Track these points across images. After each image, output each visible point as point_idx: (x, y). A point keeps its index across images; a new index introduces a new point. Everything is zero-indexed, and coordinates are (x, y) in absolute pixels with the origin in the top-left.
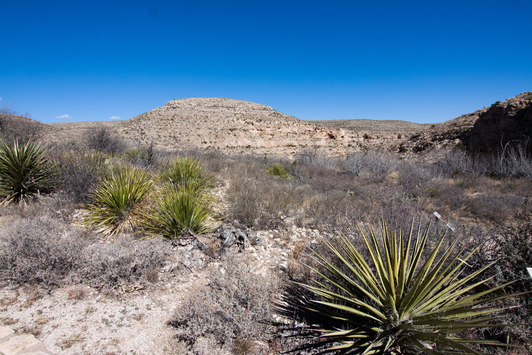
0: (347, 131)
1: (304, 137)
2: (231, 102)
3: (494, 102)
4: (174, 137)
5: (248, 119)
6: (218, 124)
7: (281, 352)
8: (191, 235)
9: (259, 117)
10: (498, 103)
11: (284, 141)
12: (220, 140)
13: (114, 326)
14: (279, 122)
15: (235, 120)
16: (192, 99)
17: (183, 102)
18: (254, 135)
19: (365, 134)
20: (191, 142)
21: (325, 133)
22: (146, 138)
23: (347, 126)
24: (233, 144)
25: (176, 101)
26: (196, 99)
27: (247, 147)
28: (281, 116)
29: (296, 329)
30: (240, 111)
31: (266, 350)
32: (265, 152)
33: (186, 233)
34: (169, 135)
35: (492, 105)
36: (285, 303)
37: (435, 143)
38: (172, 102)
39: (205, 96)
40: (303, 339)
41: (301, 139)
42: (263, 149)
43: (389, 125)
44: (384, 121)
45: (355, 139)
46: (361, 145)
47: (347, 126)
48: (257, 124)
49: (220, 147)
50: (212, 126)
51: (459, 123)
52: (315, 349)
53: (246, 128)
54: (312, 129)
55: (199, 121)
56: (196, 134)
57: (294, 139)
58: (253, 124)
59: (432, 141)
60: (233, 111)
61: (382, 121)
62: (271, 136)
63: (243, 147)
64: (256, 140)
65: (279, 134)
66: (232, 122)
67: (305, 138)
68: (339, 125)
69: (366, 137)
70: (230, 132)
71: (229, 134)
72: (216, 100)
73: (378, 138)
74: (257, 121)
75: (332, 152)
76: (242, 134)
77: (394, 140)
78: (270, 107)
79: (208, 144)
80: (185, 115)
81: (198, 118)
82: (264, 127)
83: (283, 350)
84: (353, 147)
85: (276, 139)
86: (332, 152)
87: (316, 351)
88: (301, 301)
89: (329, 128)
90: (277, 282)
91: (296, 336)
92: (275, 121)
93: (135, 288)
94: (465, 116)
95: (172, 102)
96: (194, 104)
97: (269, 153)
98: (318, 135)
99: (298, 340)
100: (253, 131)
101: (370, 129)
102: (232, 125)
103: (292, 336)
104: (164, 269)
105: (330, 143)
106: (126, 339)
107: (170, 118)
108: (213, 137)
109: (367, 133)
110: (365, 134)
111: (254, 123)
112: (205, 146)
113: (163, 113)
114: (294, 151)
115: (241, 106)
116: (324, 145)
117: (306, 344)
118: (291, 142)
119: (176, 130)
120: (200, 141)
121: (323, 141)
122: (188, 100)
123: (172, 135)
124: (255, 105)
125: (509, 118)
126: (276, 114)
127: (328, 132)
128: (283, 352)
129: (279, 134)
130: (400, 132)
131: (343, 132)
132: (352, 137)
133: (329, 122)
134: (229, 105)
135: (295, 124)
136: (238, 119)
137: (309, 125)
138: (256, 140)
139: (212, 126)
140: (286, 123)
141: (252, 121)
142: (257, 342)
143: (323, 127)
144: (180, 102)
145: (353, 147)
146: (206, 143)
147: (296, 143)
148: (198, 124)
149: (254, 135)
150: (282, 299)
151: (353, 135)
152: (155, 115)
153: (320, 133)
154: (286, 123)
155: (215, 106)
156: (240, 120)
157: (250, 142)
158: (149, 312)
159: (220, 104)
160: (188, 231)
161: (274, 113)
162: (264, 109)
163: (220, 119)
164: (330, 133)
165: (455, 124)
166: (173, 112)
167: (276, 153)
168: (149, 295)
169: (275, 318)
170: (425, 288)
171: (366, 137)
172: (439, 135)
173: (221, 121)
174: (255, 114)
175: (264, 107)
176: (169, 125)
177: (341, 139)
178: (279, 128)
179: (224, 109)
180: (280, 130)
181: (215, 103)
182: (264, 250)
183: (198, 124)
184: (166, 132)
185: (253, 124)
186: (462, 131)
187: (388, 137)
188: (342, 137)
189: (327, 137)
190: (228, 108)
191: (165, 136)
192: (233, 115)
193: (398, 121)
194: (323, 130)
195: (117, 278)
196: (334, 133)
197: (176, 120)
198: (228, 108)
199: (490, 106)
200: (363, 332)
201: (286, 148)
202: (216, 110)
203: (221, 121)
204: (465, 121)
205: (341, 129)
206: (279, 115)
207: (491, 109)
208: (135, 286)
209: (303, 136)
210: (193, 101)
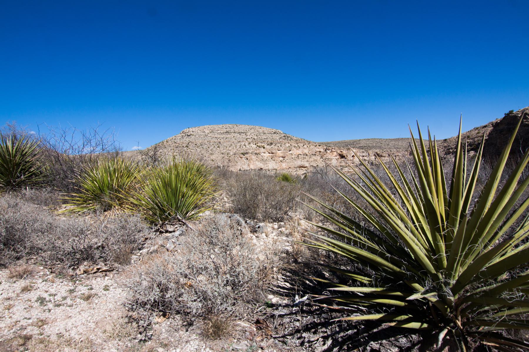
1: (314, 157)
2: (243, 128)
3: (507, 112)
5: (260, 143)
6: (230, 148)
7: (274, 336)
8: (179, 220)
9: (270, 141)
10: (511, 112)
11: (296, 163)
13: (50, 306)
14: (289, 145)
15: (247, 144)
16: (205, 126)
21: (335, 153)
25: (191, 130)
26: (210, 126)
29: (296, 305)
30: (251, 136)
31: (251, 333)
33: (175, 219)
35: (505, 114)
36: (286, 283)
37: (448, 156)
38: (186, 130)
40: (306, 317)
41: (312, 160)
44: (394, 140)
45: (366, 158)
47: (357, 146)
50: (224, 151)
51: (472, 135)
52: (324, 329)
53: (258, 152)
54: (322, 150)
55: (212, 147)
57: (305, 160)
58: (264, 148)
59: (446, 154)
60: (244, 136)
61: (392, 140)
64: (268, 162)
65: (290, 156)
66: (244, 147)
68: (348, 145)
69: (377, 155)
70: (242, 156)
72: (228, 127)
74: (268, 145)
76: (254, 157)
78: (280, 131)
81: (211, 144)
82: (275, 149)
83: (277, 333)
85: (287, 161)
87: (326, 332)
88: (308, 282)
89: (339, 148)
90: (278, 263)
91: (296, 313)
92: (285, 143)
93: (98, 269)
94: (477, 128)
95: (186, 130)
96: (207, 131)
98: (329, 155)
99: (299, 318)
100: (265, 155)
101: (380, 147)
102: (244, 149)
103: (291, 314)
104: (141, 252)
105: (340, 162)
106: (58, 320)
107: (185, 145)
109: (378, 151)
111: (265, 146)
113: (179, 141)
115: (252, 131)
117: (311, 323)
118: (302, 163)
121: (334, 160)
122: (201, 128)
124: (266, 130)
125: (525, 126)
126: (286, 137)
128: (277, 336)
129: (290, 156)
132: (363, 156)
133: (339, 143)
134: (241, 131)
135: (305, 146)
136: (250, 143)
138: (268, 162)
139: (224, 151)
140: (296, 145)
141: (263, 145)
142: (239, 322)
144: (194, 130)
147: (307, 164)
148: (212, 150)
149: (265, 158)
150: (282, 280)
151: (364, 154)
152: (170, 143)
154: (296, 145)
156: (252, 145)
157: (262, 165)
158: (105, 292)
159: (232, 130)
160: (176, 215)
161: (284, 136)
162: (274, 133)
163: (233, 144)
164: (340, 153)
165: (468, 137)
166: (188, 140)
168: (113, 276)
169: (271, 299)
170: (491, 222)
171: (377, 155)
172: (452, 148)
173: (234, 145)
175: (274, 130)
178: (290, 151)
179: (236, 134)
180: (290, 152)
181: (227, 130)
182: (265, 237)
183: (212, 150)
185: (264, 148)
186: (476, 143)
187: (399, 154)
189: (338, 157)
190: (240, 133)
192: (245, 140)
194: (333, 150)
195: (79, 259)
196: (345, 152)
197: (191, 147)
198: (240, 133)
199: (503, 116)
200: (399, 293)
201: (298, 169)
202: (229, 136)
203: (234, 145)
204: (478, 133)
206: (289, 138)
207: (504, 118)
208: (99, 267)
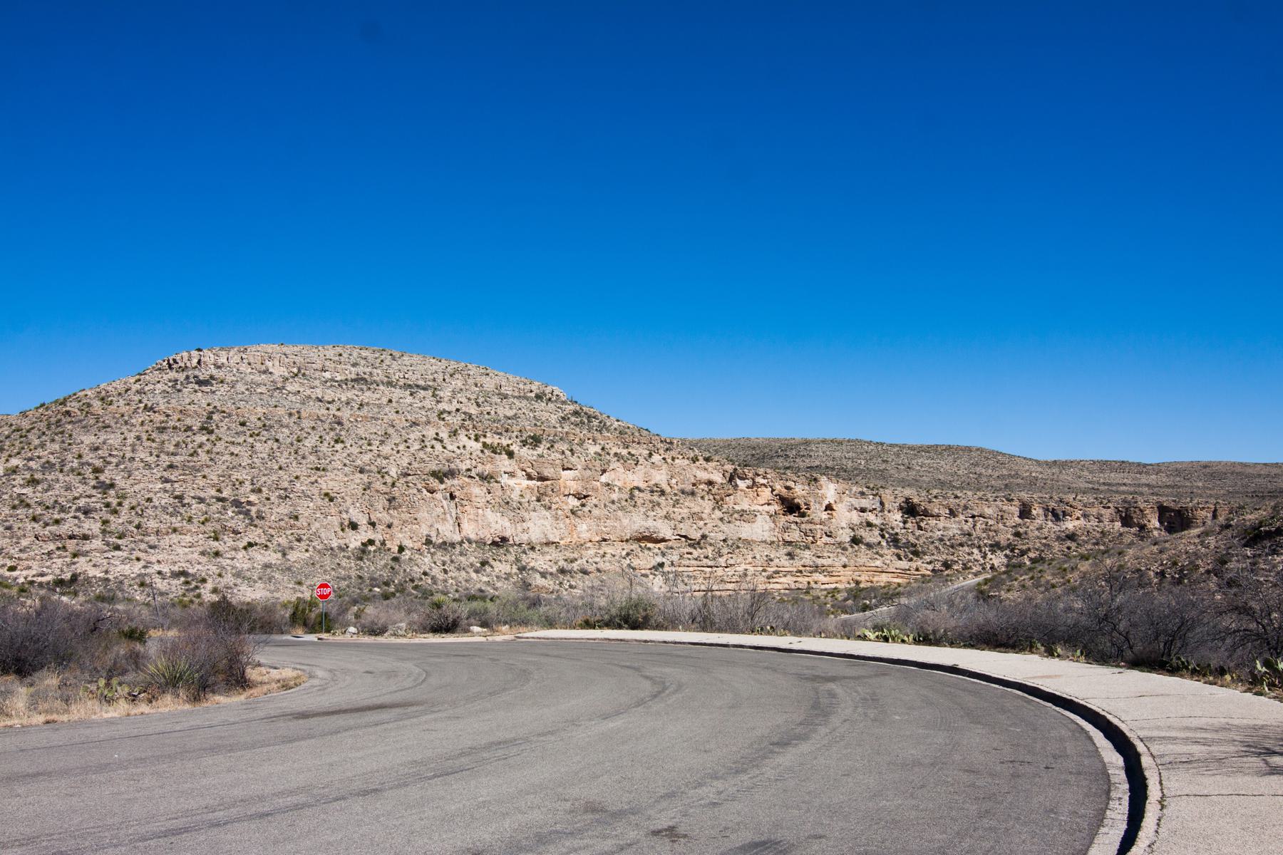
0: (842, 486)
2: (419, 366)
4: (237, 503)
6: (386, 449)
11: (625, 522)
12: (405, 516)
15: (444, 435)
17: (237, 358)
18: (515, 496)
19: (907, 500)
20: (302, 522)
21: (766, 494)
22: (126, 504)
23: (800, 463)
24: (448, 532)
25: (209, 357)
27: (494, 543)
28: (603, 427)
30: (455, 405)
32: (562, 563)
34: (213, 493)
39: (318, 340)
42: (552, 553)
43: (945, 464)
45: (871, 517)
46: (895, 541)
48: (525, 453)
49: (408, 543)
50: (366, 458)
53: (488, 469)
54: (718, 478)
56: (316, 491)
57: (661, 512)
58: (511, 455)
62: (576, 503)
63: (481, 543)
64: (526, 515)
65: (605, 495)
66: (438, 446)
67: (696, 509)
70: (434, 483)
71: (432, 492)
73: (953, 513)
74: (524, 443)
75: (797, 563)
76: (477, 490)
77: (1010, 523)
79: (364, 534)
80: (254, 412)
81: (306, 424)
84: (869, 546)
85: (596, 512)
86: (797, 563)
95: (187, 357)
96: (279, 371)
97: (575, 566)
98: (742, 500)
100: (512, 482)
108: (381, 503)
110: (907, 500)
111: (515, 448)
112: (355, 540)
114: (659, 559)
115: (458, 383)
116: (768, 536)
118: (650, 523)
119: (236, 475)
120: (335, 521)
122: (255, 352)
123: (225, 495)
124: (509, 382)
127: (779, 487)
130: (1025, 496)
131: (829, 490)
132: (863, 510)
134: (413, 378)
135: (656, 458)
137: (707, 460)
139: (366, 458)
140: (624, 452)
141: (505, 442)
143: (761, 471)
145: (869, 546)
146: (354, 526)
147: (665, 530)
149: (515, 496)
151: (865, 503)
153: (751, 493)
154: (624, 452)
155: (358, 380)
157: (507, 524)
161: (576, 413)
162: (538, 397)
163: (391, 431)
164: (784, 492)
166: (202, 399)
167: (601, 566)
171: (910, 510)
174: (510, 413)
176: (702, 523)
177: (824, 516)
178: (604, 471)
179: (397, 393)
180: (604, 479)
181: (360, 369)
183: (315, 451)
184: (201, 482)
185: (511, 455)
187: (988, 511)
188: (829, 508)
189: (776, 507)
190: (412, 388)
191: (201, 500)
193: (969, 449)
194: (760, 480)
196: (800, 491)
198: (412, 388)
201: (635, 546)
202: (367, 396)
205: (823, 480)
206: (596, 423)
209: (688, 502)
210: (277, 358)
